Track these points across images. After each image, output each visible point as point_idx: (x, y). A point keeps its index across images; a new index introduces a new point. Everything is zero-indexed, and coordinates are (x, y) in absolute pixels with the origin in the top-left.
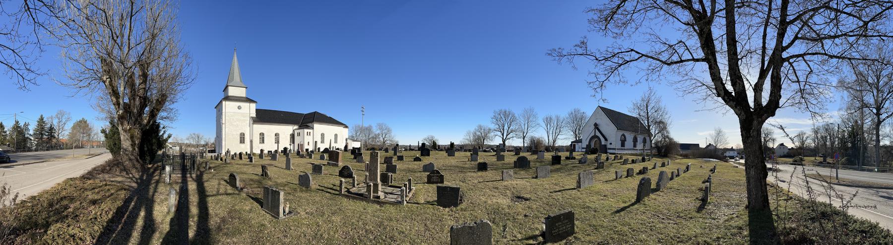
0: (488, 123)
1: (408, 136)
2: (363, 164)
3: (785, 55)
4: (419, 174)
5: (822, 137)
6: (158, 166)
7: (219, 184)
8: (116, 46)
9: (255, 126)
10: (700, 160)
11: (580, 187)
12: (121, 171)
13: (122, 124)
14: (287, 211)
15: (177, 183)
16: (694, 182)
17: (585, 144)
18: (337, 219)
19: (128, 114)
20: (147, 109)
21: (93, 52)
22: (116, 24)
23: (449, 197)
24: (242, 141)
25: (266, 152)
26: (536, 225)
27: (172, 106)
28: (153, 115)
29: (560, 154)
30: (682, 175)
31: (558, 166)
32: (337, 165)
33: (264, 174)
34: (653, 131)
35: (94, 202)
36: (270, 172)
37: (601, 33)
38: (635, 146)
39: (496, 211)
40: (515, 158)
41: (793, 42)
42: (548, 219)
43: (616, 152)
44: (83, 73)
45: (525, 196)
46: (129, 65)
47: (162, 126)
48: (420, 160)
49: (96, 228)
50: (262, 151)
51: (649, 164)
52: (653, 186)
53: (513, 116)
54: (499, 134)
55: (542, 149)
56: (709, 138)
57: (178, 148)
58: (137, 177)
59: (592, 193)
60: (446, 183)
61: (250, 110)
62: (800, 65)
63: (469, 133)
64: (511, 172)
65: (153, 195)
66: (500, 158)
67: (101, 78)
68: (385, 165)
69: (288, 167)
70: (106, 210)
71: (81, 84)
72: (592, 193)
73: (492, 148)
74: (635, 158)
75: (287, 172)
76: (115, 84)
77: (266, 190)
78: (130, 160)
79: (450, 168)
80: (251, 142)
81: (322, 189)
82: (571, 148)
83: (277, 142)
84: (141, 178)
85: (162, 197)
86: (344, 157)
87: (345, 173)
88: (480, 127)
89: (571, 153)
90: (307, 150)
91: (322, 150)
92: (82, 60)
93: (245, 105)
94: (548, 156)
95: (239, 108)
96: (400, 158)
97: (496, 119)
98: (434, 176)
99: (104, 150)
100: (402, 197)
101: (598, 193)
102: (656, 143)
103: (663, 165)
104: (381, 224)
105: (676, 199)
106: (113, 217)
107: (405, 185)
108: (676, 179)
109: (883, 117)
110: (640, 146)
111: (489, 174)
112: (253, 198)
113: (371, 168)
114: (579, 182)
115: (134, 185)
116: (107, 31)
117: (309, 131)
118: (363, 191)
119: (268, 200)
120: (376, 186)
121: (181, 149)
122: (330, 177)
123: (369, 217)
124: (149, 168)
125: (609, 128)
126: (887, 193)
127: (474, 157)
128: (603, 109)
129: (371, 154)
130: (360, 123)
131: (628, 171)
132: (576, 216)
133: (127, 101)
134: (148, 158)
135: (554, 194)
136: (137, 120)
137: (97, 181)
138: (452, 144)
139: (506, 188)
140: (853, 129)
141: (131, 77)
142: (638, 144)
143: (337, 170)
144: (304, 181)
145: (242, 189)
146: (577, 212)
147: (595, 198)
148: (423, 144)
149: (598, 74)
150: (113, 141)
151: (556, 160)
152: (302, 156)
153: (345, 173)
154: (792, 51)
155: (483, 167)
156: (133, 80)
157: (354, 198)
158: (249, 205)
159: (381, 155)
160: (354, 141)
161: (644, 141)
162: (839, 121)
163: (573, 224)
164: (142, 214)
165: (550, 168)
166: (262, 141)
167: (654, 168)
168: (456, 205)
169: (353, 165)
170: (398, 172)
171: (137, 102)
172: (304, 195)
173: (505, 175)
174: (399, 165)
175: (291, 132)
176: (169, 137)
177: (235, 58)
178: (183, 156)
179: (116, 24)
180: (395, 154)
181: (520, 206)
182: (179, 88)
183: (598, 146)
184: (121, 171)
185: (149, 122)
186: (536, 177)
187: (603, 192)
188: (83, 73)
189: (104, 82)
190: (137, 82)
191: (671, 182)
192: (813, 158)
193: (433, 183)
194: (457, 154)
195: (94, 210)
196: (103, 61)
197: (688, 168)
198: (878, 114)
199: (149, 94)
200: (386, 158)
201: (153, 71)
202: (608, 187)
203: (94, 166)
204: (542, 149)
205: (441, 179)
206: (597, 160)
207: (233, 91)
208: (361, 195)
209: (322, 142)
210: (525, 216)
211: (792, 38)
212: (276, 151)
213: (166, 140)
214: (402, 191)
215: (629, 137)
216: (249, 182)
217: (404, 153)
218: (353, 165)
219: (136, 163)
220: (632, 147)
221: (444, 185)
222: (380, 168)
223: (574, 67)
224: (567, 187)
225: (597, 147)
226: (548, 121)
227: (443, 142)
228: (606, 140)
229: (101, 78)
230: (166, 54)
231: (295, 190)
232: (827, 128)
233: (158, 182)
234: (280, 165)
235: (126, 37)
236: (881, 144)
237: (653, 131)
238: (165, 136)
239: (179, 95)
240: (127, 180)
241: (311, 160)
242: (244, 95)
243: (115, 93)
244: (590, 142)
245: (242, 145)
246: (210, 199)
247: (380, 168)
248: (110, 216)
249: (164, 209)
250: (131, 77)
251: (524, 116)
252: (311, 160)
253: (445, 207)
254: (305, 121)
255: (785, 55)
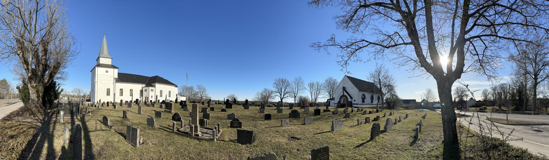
0: (271, 87)
1: (218, 95)
2: (188, 112)
3: (467, 36)
4: (224, 121)
5: (498, 93)
6: (54, 111)
7: (96, 123)
8: (27, 31)
9: (117, 84)
10: (416, 110)
11: (333, 130)
12: (30, 115)
13: (31, 83)
14: (141, 142)
15: (68, 123)
16: (410, 125)
17: (336, 101)
18: (171, 148)
19: (34, 76)
20: (47, 72)
21: (11, 35)
22: (27, 16)
23: (245, 138)
24: (108, 93)
25: (124, 102)
26: (305, 156)
27: (63, 70)
28: (51, 76)
29: (319, 108)
30: (403, 120)
31: (319, 116)
32: (170, 112)
33: (125, 116)
34: (384, 92)
35: (12, 137)
36: (129, 115)
37: (346, 30)
38: (372, 102)
39: (278, 147)
40: (290, 111)
41: (473, 27)
42: (313, 151)
43: (359, 106)
44: (4, 49)
45: (297, 137)
46: (36, 43)
47: (57, 84)
48: (225, 111)
49: (14, 155)
50: (121, 101)
51: (381, 114)
52: (382, 128)
53: (288, 82)
54: (279, 94)
55: (308, 105)
56: (423, 95)
57: (66, 98)
58: (41, 118)
59: (341, 134)
60: (243, 128)
61: (114, 73)
62: (478, 43)
63: (258, 94)
64: (288, 121)
65: (53, 132)
66: (280, 111)
67: (16, 53)
68: (202, 114)
69: (139, 112)
70: (21, 142)
71: (3, 56)
72: (341, 134)
73: (274, 104)
74: (371, 110)
75: (139, 115)
76: (26, 56)
77: (129, 127)
78: (36, 107)
79: (246, 118)
80: (114, 94)
81: (162, 128)
82: (327, 104)
83: (132, 95)
84: (44, 119)
85: (59, 133)
86: (175, 107)
87: (176, 118)
88: (266, 90)
89: (327, 107)
90: (151, 101)
91: (160, 101)
92: (4, 40)
93: (111, 70)
94: (312, 109)
95: (107, 72)
96: (212, 109)
97: (276, 84)
98: (235, 123)
99: (18, 100)
100: (214, 136)
101: (345, 134)
102: (387, 100)
103: (391, 114)
104: (199, 154)
105: (398, 137)
106: (26, 148)
107: (216, 128)
108: (398, 124)
109: (539, 80)
110: (375, 102)
111: (272, 122)
112: (119, 133)
113: (193, 115)
114: (332, 127)
115: (39, 124)
116: (21, 21)
117: (152, 88)
118: (188, 130)
119: (130, 135)
120: (196, 127)
121: (69, 99)
122: (166, 120)
123: (191, 148)
124: (49, 113)
125: (353, 90)
126: (538, 128)
127: (262, 111)
128: (349, 77)
129: (193, 105)
130: (186, 85)
131: (366, 119)
132: (330, 150)
133: (34, 67)
134: (48, 105)
135: (316, 135)
136: (40, 80)
137: (14, 122)
138: (247, 101)
139: (284, 131)
140: (520, 87)
141: (36, 51)
142: (374, 100)
143: (171, 116)
144: (150, 122)
145: (111, 127)
146: (331, 147)
147: (343, 138)
148: (228, 100)
149: (343, 56)
150: (24, 94)
151: (317, 112)
152: (148, 105)
153: (176, 118)
154: (472, 33)
155: (268, 117)
156: (38, 54)
157: (182, 135)
158: (117, 138)
159: (199, 106)
160: (182, 96)
161: (379, 98)
162: (510, 82)
163: (329, 155)
164: (46, 145)
165: (313, 117)
166: (122, 94)
167: (384, 116)
168: (250, 143)
169: (181, 112)
170: (210, 119)
171: (41, 68)
172: (150, 132)
173: (283, 122)
174: (211, 114)
175: (141, 89)
176: (62, 91)
177: (105, 39)
178: (70, 103)
179: (27, 16)
180: (209, 106)
181: (294, 143)
182: (69, 58)
183: (346, 102)
184: (30, 115)
185: (49, 81)
186: (304, 124)
187: (350, 132)
188: (4, 49)
189: (19, 55)
190: (40, 54)
191: (395, 126)
192: (491, 107)
193: (234, 127)
194: (250, 107)
195: (12, 143)
196: (18, 41)
197: (407, 116)
198: (536, 79)
199: (48, 62)
200: (203, 109)
201: (51, 47)
202: (352, 130)
203: (11, 111)
204: (308, 105)
205: (240, 125)
206: (345, 112)
207: (103, 61)
208: (187, 133)
209: (161, 96)
210: (298, 150)
211: (472, 25)
212: (131, 101)
213: (60, 93)
214: (213, 132)
215: (368, 96)
216: (115, 122)
217: (215, 106)
218: (181, 112)
219: (40, 109)
220: (370, 103)
221: (242, 129)
222: (199, 116)
223: (328, 53)
224: (325, 131)
225: (345, 103)
226: (311, 86)
227: (241, 98)
228: (351, 98)
229: (16, 53)
230: (60, 36)
231: (145, 128)
232: (502, 87)
233: (55, 122)
234: (134, 111)
235: (33, 26)
236: (538, 97)
237: (384, 90)
238: (60, 90)
239: (69, 63)
240: (34, 121)
241: (154, 108)
242: (110, 63)
243: (26, 62)
244: (340, 100)
245: (108, 97)
246: (91, 134)
247: (199, 116)
248: (24, 147)
249: (61, 139)
250: (36, 51)
251: (295, 83)
252: (154, 108)
253: (242, 144)
254: (150, 82)
255: (467, 36)
